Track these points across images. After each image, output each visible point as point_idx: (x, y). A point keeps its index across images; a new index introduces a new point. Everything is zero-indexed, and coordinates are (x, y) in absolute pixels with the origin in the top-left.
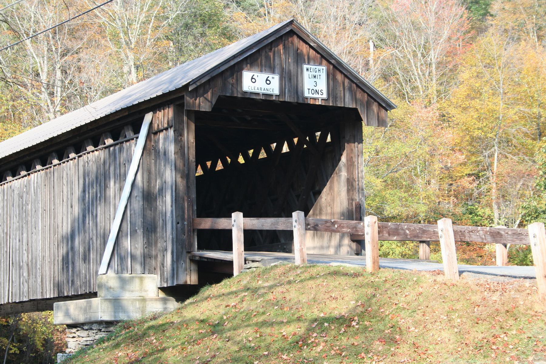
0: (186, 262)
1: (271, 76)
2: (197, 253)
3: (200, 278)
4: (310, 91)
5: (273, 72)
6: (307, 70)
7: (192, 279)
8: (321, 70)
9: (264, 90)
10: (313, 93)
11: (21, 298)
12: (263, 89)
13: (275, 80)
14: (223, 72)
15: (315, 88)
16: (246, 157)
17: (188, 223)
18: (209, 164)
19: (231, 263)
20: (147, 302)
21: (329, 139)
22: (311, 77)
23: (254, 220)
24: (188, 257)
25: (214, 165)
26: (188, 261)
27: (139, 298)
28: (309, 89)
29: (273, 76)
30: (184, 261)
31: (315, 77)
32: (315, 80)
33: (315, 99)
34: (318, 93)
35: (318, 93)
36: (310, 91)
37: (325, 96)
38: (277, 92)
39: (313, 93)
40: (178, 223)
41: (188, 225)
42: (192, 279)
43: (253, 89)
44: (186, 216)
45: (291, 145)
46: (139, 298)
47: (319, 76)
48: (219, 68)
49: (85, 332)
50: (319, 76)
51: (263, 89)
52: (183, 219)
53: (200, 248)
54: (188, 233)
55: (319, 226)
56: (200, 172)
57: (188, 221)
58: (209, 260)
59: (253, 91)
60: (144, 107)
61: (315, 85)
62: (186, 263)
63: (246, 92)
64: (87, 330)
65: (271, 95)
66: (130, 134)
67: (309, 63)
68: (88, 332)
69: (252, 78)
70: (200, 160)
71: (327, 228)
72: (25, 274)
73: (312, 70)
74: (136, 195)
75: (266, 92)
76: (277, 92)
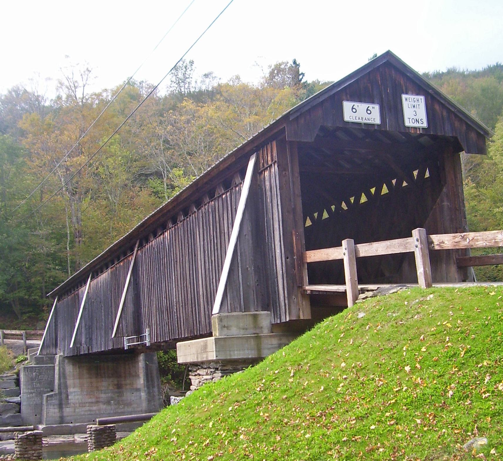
0: (298, 297)
1: (371, 106)
2: (309, 288)
3: (313, 313)
4: (411, 120)
5: (373, 102)
6: (406, 99)
7: (305, 314)
8: (420, 100)
9: (366, 119)
10: (413, 120)
11: (159, 338)
12: (364, 119)
13: (375, 109)
14: (322, 102)
15: (415, 118)
16: (348, 203)
17: (297, 257)
18: (316, 215)
19: (345, 293)
20: (262, 339)
21: (427, 175)
22: (410, 106)
23: (366, 245)
24: (299, 292)
25: (320, 215)
26: (299, 295)
27: (253, 335)
28: (409, 118)
29: (373, 106)
30: (295, 296)
31: (414, 107)
32: (414, 109)
33: (415, 128)
34: (418, 122)
35: (418, 122)
36: (411, 120)
37: (425, 125)
38: (378, 121)
39: (413, 122)
40: (288, 258)
41: (297, 259)
42: (305, 314)
43: (354, 118)
44: (295, 251)
45: (389, 186)
46: (253, 335)
47: (418, 106)
48: (319, 97)
49: (204, 370)
50: (418, 106)
51: (364, 119)
52: (292, 253)
53: (311, 283)
54: (298, 268)
55: (446, 243)
56: (309, 223)
57: (297, 255)
58: (320, 293)
59: (354, 121)
60: (248, 149)
61: (415, 114)
62: (297, 299)
63: (348, 123)
64: (205, 369)
65: (373, 125)
66: (237, 180)
67: (407, 93)
68: (206, 370)
69: (353, 108)
70: (307, 213)
71: (456, 244)
72: (166, 317)
73: (411, 100)
74: (245, 234)
75: (367, 122)
76: (378, 121)
